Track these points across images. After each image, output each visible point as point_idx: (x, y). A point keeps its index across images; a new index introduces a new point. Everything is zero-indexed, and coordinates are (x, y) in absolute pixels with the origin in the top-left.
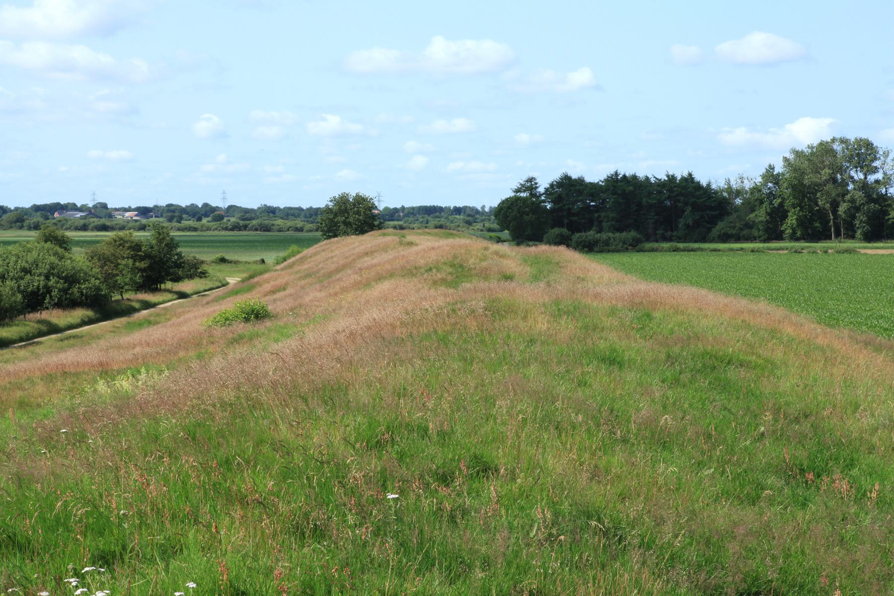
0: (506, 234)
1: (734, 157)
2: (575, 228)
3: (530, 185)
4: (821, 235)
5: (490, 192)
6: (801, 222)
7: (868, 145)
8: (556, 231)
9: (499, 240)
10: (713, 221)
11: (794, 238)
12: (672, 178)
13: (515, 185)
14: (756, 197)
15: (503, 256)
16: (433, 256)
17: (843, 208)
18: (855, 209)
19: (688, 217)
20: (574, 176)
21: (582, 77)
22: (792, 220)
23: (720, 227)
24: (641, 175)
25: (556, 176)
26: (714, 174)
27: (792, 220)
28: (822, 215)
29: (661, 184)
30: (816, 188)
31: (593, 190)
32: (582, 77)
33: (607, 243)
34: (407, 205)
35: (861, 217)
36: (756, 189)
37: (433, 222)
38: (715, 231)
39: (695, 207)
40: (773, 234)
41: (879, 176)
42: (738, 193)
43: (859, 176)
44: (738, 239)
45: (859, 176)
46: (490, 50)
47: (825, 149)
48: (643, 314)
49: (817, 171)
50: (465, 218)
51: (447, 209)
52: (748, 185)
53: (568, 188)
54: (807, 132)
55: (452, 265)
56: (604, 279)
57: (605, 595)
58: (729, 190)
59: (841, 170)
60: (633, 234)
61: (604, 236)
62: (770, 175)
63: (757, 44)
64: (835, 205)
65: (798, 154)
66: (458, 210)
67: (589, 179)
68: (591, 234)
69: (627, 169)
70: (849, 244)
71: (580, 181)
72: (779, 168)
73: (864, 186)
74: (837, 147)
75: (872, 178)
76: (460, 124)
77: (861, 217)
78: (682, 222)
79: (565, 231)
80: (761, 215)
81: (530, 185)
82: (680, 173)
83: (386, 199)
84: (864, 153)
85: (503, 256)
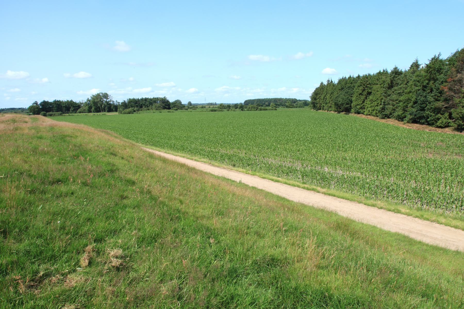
0: (31, 113)
1: (81, 96)
2: (47, 111)
3: (36, 103)
4: (99, 111)
5: (27, 104)
6: (95, 109)
7: (107, 94)
8: (43, 112)
9: (30, 115)
10: (77, 109)
11: (94, 112)
12: (68, 101)
13: (33, 103)
14: (86, 104)
15: (26, 118)
16: (8, 118)
17: (103, 106)
18: (105, 106)
19: (72, 109)
20: (46, 101)
21: (45, 80)
22: (93, 109)
23: (79, 110)
24: (61, 100)
25: (42, 101)
26: (77, 100)
27: (93, 109)
28: (99, 107)
29: (66, 102)
30: (97, 103)
31: (51, 104)
32: (45, 80)
33: (55, 114)
34: (7, 108)
35: (106, 108)
36: (86, 103)
37: (13, 111)
38: (78, 111)
39: (73, 107)
40: (90, 111)
41: (109, 100)
42: (82, 104)
43: (105, 100)
44: (83, 112)
45: (105, 100)
46: (23, 74)
47: (98, 95)
48: (52, 128)
49: (97, 99)
50: (22, 110)
51: (17, 109)
52: (84, 102)
53: (45, 103)
54: (95, 92)
55: (12, 120)
56: (46, 121)
57: (463, 184)
58: (80, 103)
59: (102, 99)
60: (60, 112)
61: (54, 113)
62: (88, 100)
63: (82, 74)
64: (101, 106)
65: (94, 96)
66: (19, 109)
67: (49, 101)
68: (51, 113)
69: (58, 99)
70: (104, 113)
71: (48, 102)
72: (90, 99)
73: (106, 102)
74: (101, 94)
75: (108, 100)
76: (17, 90)
77: (106, 108)
78: (71, 110)
79: (45, 112)
80: (87, 108)
81: (36, 103)
82: (69, 100)
83: (184, 102)
84: (106, 96)
85: (26, 118)
